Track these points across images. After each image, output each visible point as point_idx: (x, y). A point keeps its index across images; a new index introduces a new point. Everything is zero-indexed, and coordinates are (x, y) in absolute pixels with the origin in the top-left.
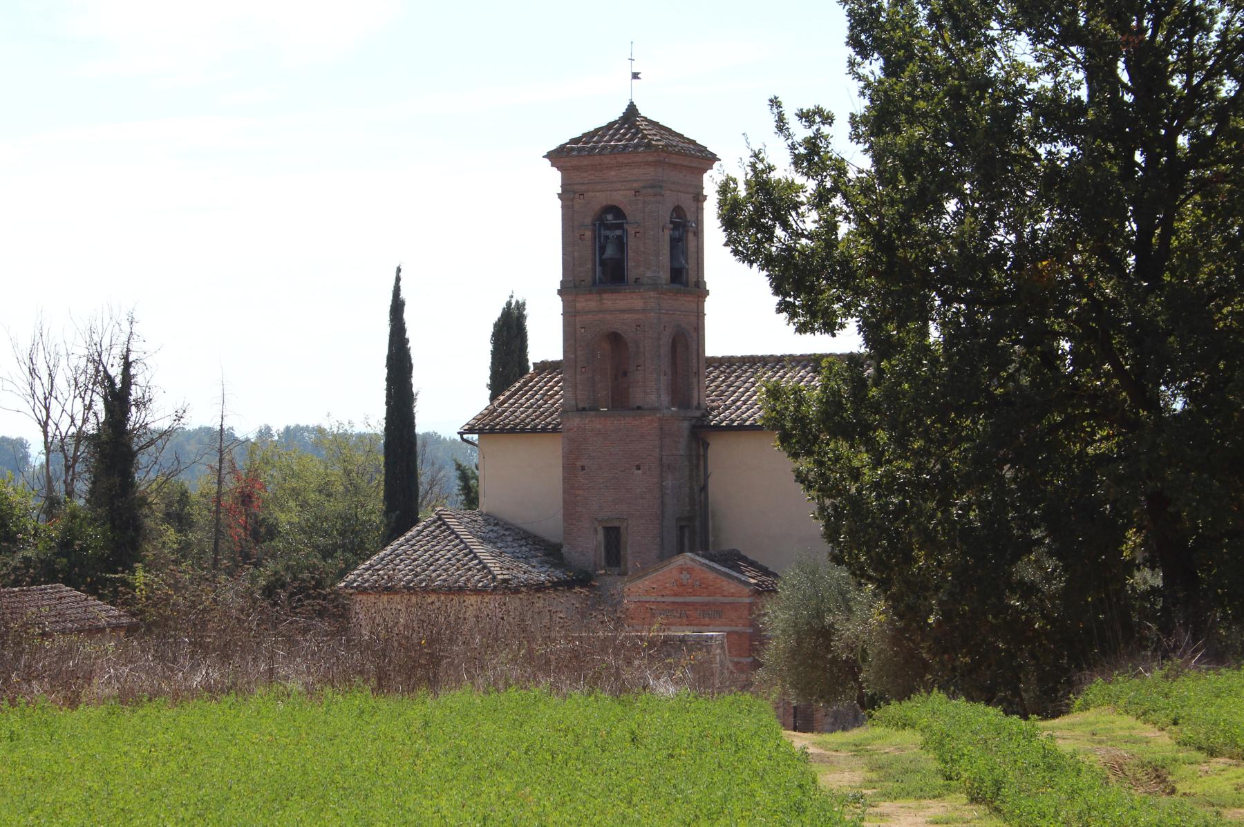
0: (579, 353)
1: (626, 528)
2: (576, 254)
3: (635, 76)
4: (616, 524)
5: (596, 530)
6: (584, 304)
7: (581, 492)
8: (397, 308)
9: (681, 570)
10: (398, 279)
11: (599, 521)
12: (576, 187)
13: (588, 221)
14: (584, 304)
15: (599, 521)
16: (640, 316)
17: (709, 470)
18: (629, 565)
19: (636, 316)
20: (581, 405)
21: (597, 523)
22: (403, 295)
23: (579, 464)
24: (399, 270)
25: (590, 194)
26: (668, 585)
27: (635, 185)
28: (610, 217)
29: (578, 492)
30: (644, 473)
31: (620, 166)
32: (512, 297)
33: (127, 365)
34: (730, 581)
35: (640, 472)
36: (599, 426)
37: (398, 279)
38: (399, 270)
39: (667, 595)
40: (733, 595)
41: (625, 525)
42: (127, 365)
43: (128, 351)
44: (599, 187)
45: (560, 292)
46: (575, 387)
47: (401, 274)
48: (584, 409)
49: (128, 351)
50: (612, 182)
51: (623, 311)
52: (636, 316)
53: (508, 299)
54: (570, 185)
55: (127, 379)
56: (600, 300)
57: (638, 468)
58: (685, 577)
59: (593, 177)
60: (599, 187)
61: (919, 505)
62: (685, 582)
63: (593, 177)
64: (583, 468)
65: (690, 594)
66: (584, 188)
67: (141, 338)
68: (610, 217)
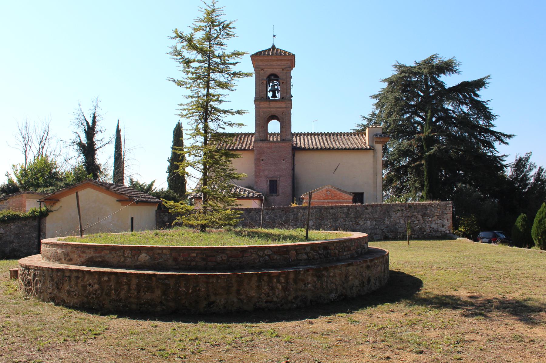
0: (261, 121)
1: (279, 180)
2: (260, 89)
3: (274, 36)
4: (275, 179)
5: (267, 181)
6: (263, 105)
7: (262, 168)
8: (118, 131)
9: (327, 190)
10: (118, 123)
11: (269, 178)
12: (261, 67)
13: (265, 78)
14: (263, 105)
15: (269, 178)
16: (284, 110)
17: (295, 163)
18: (280, 192)
19: (283, 110)
20: (261, 139)
21: (268, 179)
22: (120, 128)
23: (261, 158)
24: (118, 121)
25: (266, 69)
26: (321, 196)
27: (283, 67)
28: (273, 77)
29: (260, 168)
30: (286, 162)
31: (278, 60)
32: (179, 121)
33: (94, 117)
34: (346, 194)
35: (284, 161)
36: (269, 146)
37: (118, 123)
38: (118, 121)
39: (321, 199)
40: (346, 199)
41: (279, 179)
42: (94, 117)
43: (95, 113)
44: (269, 67)
45: (255, 101)
46: (260, 132)
47: (119, 122)
48: (262, 140)
49: (95, 113)
50: (274, 66)
51: (278, 108)
52: (283, 110)
53: (178, 121)
54: (259, 66)
55: (94, 122)
56: (269, 104)
57: (284, 160)
58: (328, 193)
59: (267, 64)
60: (269, 67)
61: (191, 199)
62: (328, 195)
63: (267, 64)
64: (263, 160)
65: (330, 199)
66: (263, 67)
67: (100, 108)
68: (273, 77)
